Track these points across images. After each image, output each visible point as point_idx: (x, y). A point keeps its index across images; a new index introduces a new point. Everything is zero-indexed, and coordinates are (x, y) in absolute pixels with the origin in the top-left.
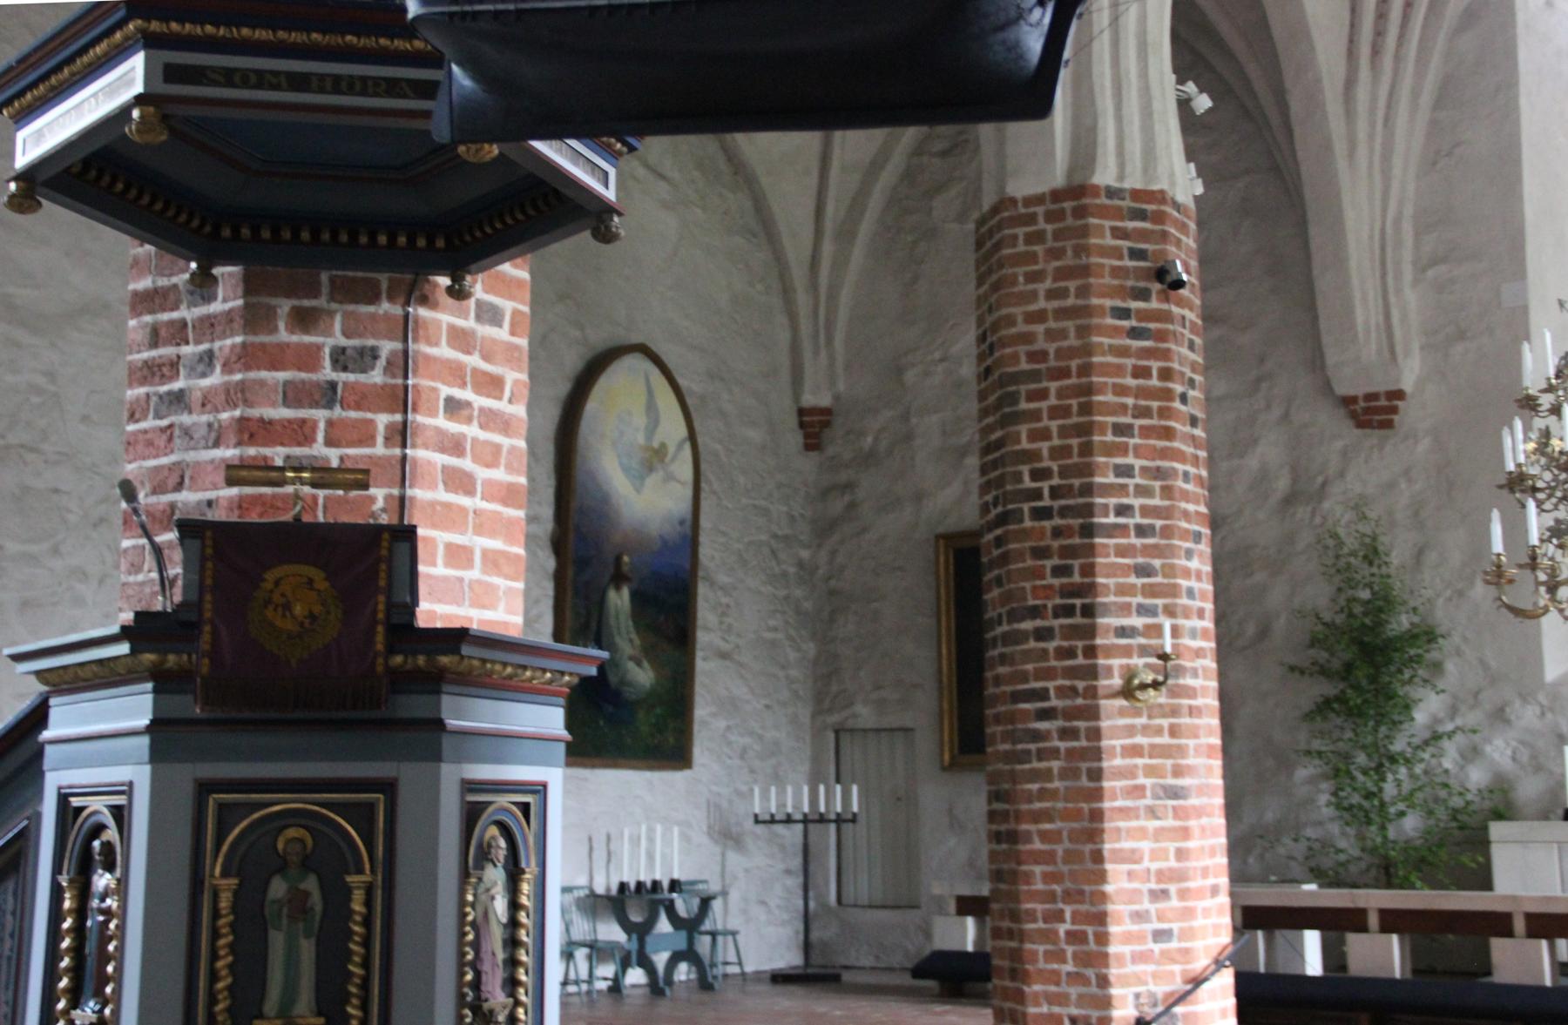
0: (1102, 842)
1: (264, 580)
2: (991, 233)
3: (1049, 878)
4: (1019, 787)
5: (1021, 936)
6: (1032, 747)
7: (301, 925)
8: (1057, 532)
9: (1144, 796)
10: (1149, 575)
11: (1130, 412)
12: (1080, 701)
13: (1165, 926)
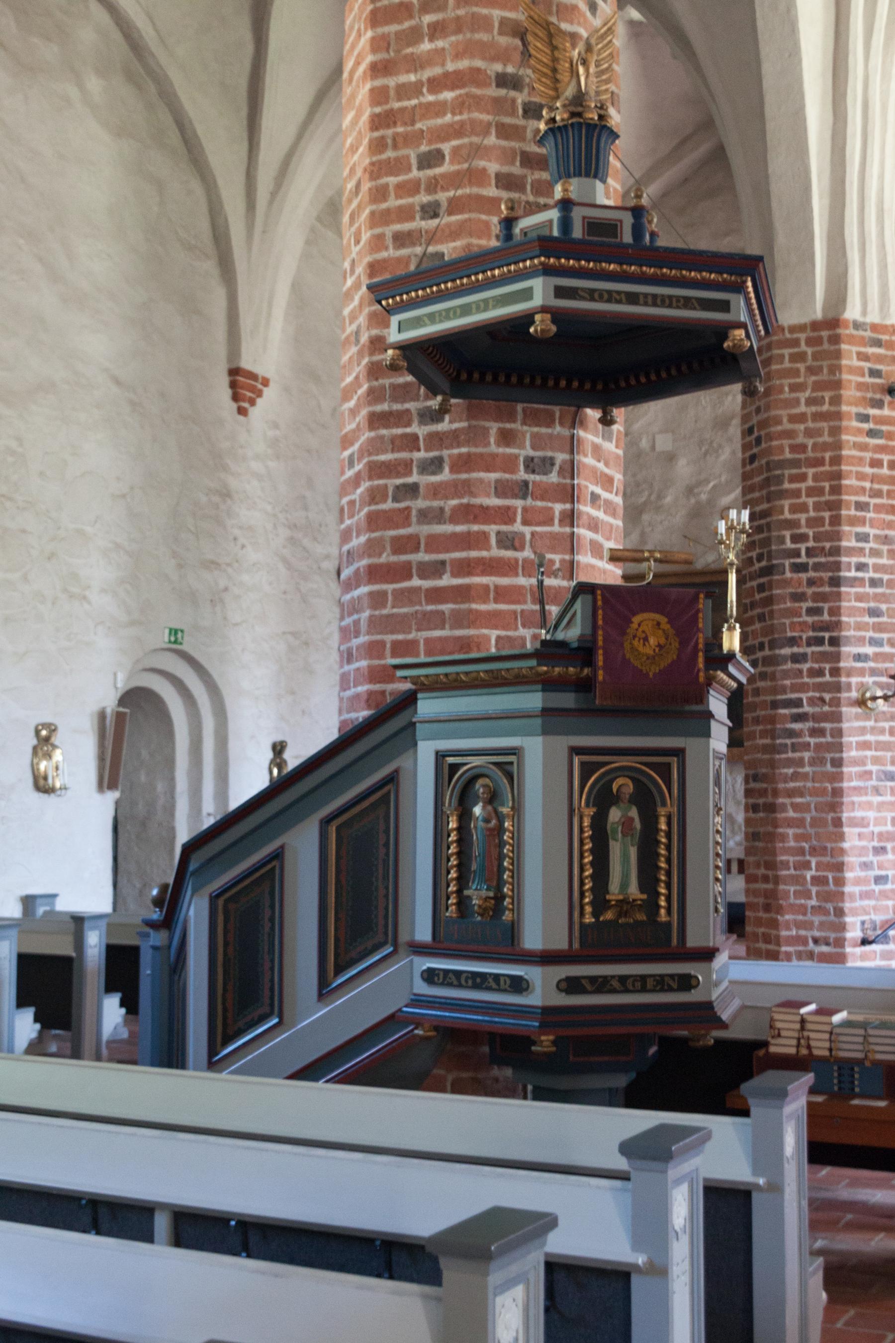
0: (842, 812)
1: (632, 622)
3: (798, 838)
4: (777, 771)
5: (777, 880)
6: (788, 742)
8: (811, 582)
9: (871, 779)
10: (878, 616)
11: (867, 493)
12: (826, 708)
13: (883, 873)
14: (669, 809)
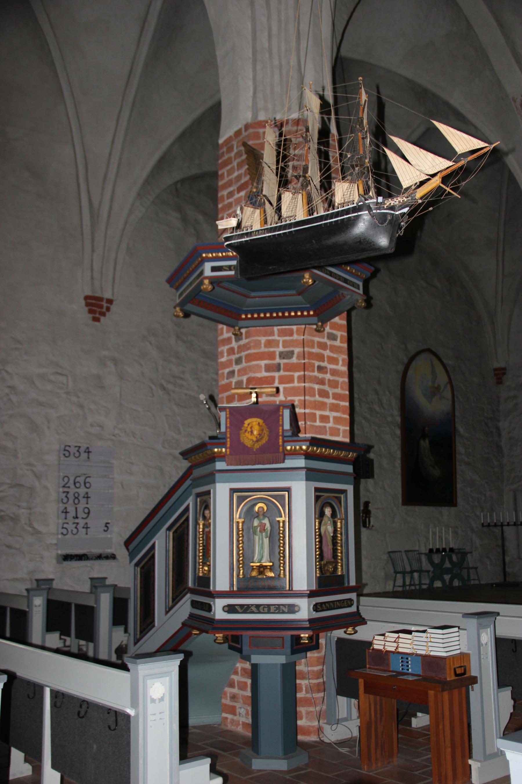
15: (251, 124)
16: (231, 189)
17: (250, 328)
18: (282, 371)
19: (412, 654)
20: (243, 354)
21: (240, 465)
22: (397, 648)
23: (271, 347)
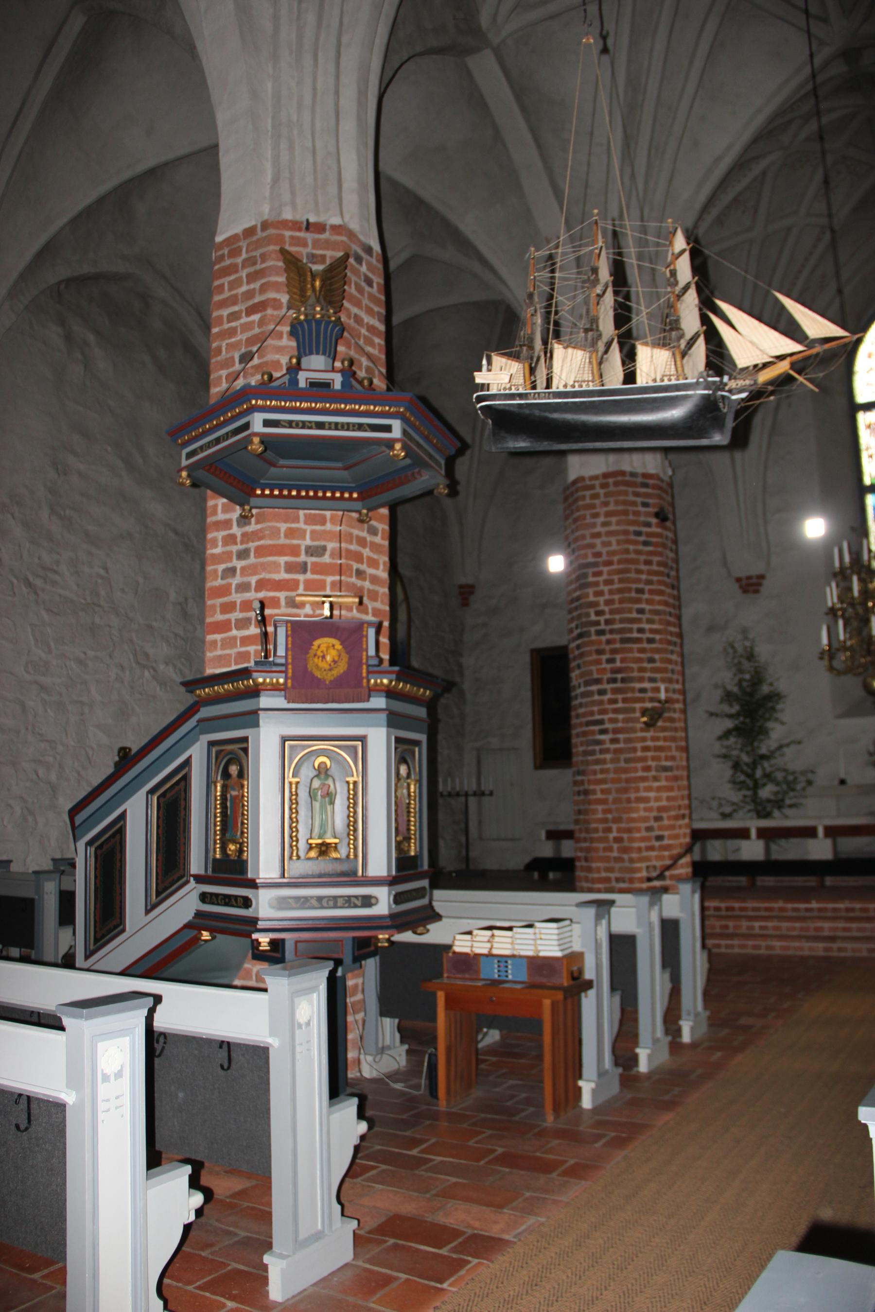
2: (572, 494)
7: (327, 799)
8: (609, 642)
14: (355, 778)
15: (272, 222)
16: (236, 308)
17: (265, 509)
18: (309, 572)
19: (513, 956)
20: (252, 545)
21: (306, 702)
22: (491, 949)
23: (294, 538)
